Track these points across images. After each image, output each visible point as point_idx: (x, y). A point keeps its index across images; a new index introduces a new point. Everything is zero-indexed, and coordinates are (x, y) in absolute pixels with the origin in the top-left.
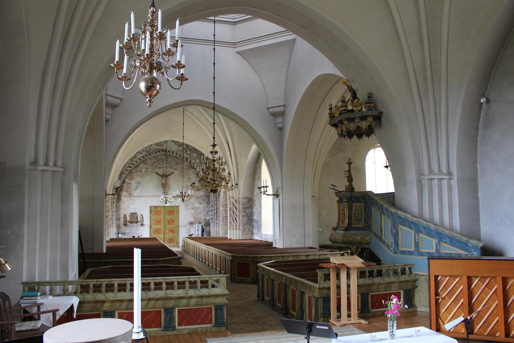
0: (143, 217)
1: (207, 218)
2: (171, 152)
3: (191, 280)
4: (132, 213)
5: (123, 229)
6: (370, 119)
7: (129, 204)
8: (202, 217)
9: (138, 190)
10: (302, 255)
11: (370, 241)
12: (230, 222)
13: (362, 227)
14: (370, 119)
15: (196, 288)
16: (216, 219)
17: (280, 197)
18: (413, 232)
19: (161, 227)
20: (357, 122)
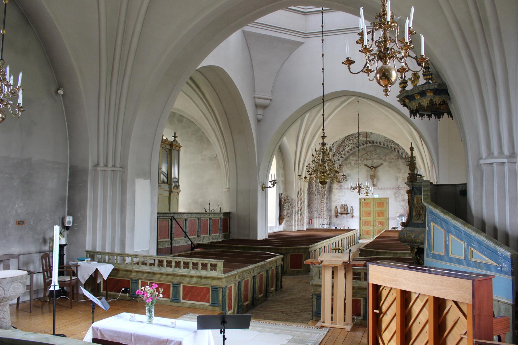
0: (353, 209)
2: (378, 143)
3: (193, 261)
4: (342, 205)
5: (334, 220)
6: (430, 94)
13: (421, 224)
14: (430, 94)
15: (197, 269)
19: (371, 219)
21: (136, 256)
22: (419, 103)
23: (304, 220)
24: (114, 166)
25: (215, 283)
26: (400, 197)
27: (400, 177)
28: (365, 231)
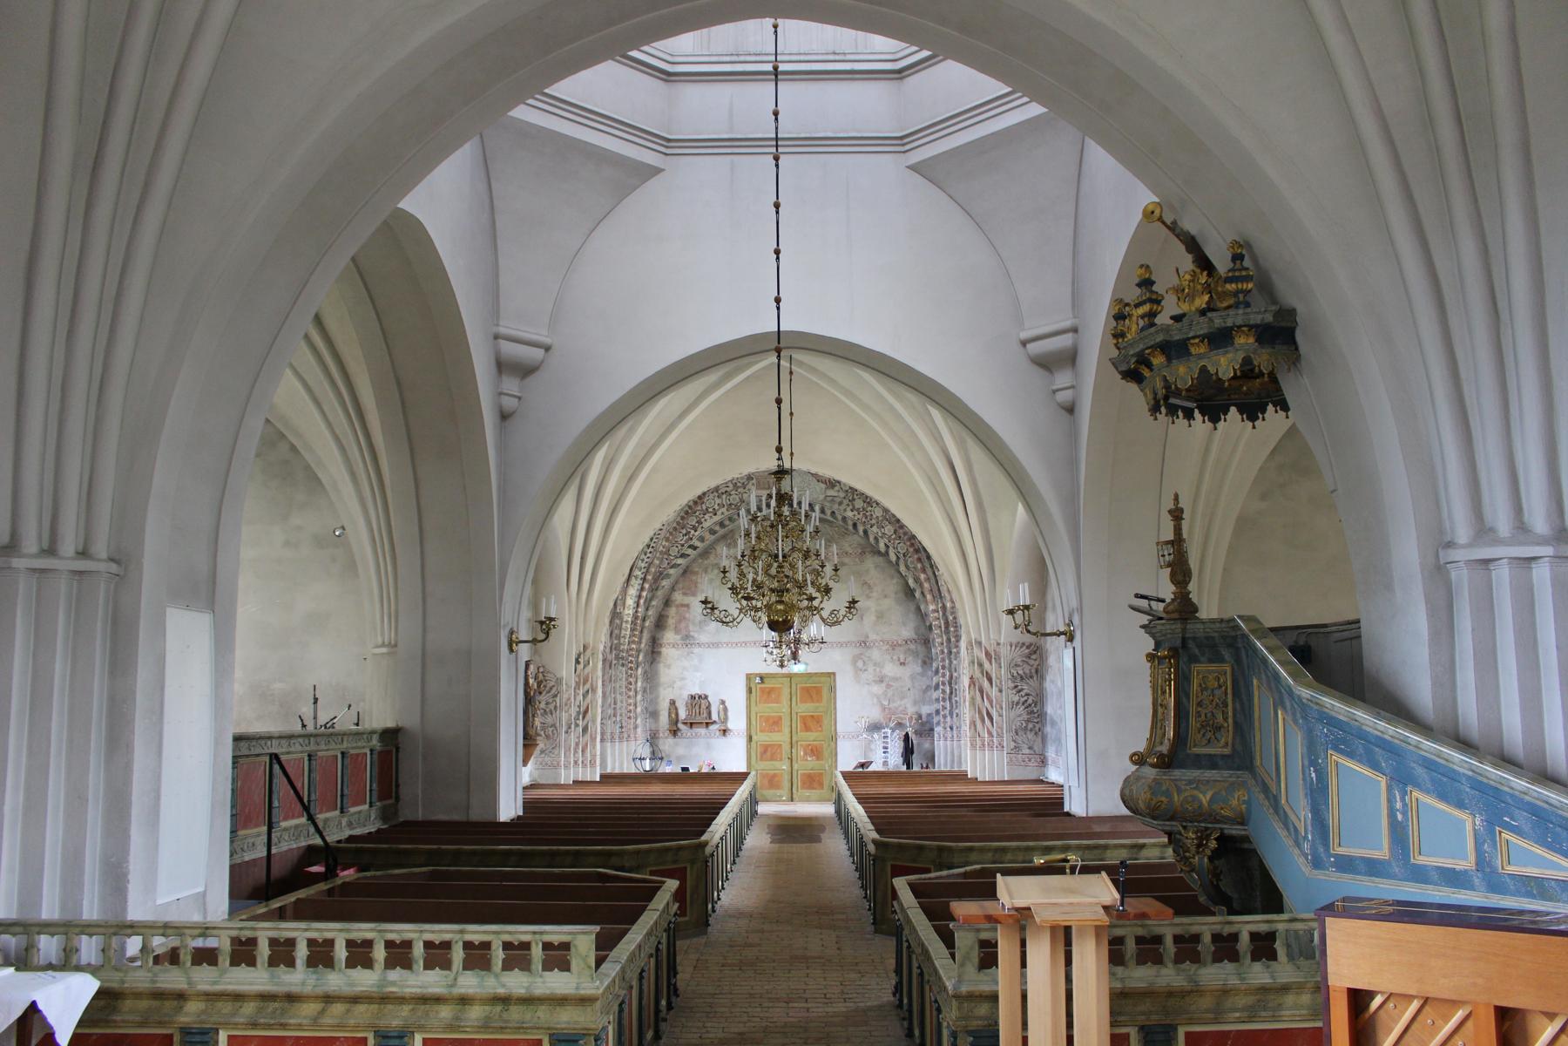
0: (725, 710)
1: (926, 710)
3: (468, 937)
4: (693, 697)
6: (1244, 341)
7: (684, 668)
8: (909, 708)
10: (1117, 847)
11: (1249, 810)
12: (973, 723)
13: (1223, 757)
14: (1244, 341)
16: (951, 714)
17: (1077, 642)
18: (1383, 782)
19: (781, 737)
20: (1200, 357)
21: (166, 928)
22: (1204, 370)
23: (594, 747)
24: (83, 554)
26: (871, 669)
28: (764, 776)
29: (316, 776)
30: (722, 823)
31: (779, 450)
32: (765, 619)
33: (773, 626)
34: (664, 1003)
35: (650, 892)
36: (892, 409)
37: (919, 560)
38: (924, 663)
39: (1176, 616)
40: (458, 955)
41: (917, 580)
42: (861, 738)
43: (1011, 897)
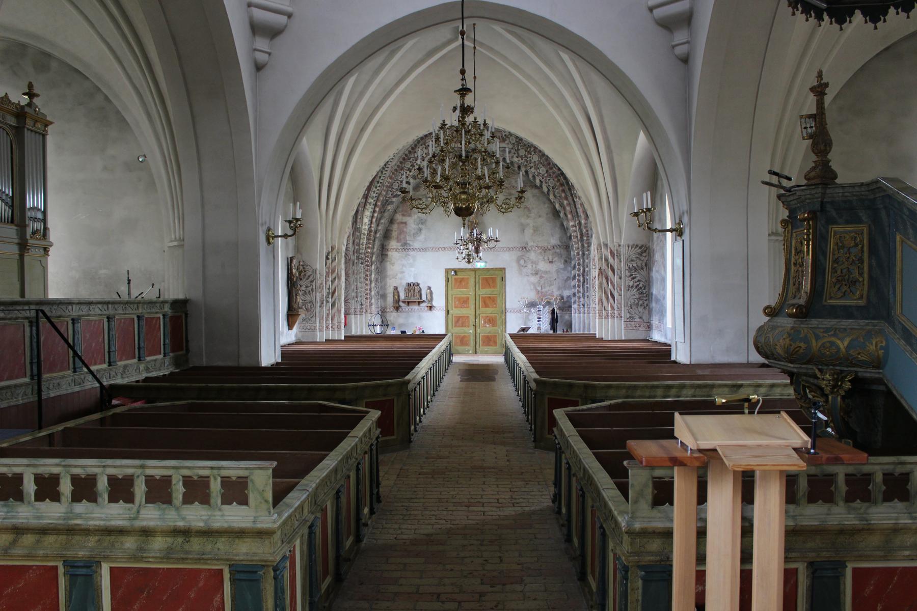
0: (431, 293)
1: (566, 293)
3: (149, 472)
4: (409, 285)
7: (403, 265)
8: (555, 291)
9: (421, 237)
12: (601, 301)
13: (858, 308)
17: (686, 236)
19: (469, 311)
23: (340, 316)
25: (245, 550)
27: (528, 224)
28: (457, 337)
29: (115, 333)
30: (424, 366)
31: (463, 72)
32: (452, 207)
33: (459, 212)
34: (366, 510)
35: (353, 421)
36: (547, 78)
37: (563, 191)
38: (566, 261)
39: (817, 181)
40: (140, 489)
41: (561, 205)
42: (522, 310)
43: (696, 439)
